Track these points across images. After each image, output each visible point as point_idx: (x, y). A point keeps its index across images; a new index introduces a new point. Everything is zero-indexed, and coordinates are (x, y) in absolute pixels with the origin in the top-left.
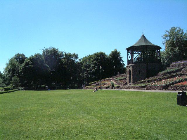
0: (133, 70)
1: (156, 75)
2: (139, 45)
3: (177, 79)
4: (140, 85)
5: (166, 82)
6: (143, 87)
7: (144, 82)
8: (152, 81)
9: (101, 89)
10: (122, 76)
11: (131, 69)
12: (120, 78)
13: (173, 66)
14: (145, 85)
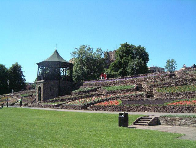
0: (43, 87)
1: (69, 94)
2: (51, 61)
3: (95, 99)
4: (53, 104)
5: (84, 102)
6: (57, 106)
7: (57, 101)
8: (65, 100)
9: (8, 106)
10: (27, 93)
11: (42, 85)
12: (25, 95)
13: (86, 85)
14: (59, 103)
